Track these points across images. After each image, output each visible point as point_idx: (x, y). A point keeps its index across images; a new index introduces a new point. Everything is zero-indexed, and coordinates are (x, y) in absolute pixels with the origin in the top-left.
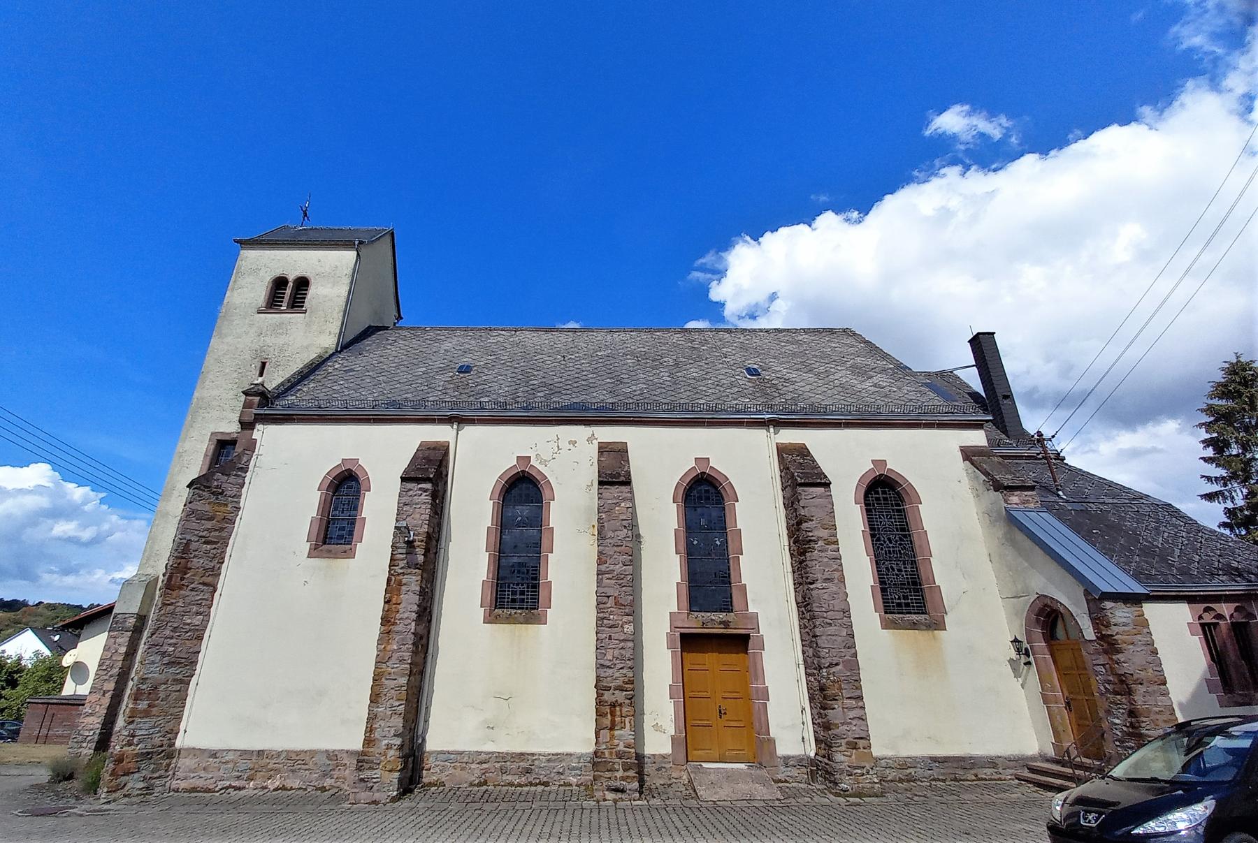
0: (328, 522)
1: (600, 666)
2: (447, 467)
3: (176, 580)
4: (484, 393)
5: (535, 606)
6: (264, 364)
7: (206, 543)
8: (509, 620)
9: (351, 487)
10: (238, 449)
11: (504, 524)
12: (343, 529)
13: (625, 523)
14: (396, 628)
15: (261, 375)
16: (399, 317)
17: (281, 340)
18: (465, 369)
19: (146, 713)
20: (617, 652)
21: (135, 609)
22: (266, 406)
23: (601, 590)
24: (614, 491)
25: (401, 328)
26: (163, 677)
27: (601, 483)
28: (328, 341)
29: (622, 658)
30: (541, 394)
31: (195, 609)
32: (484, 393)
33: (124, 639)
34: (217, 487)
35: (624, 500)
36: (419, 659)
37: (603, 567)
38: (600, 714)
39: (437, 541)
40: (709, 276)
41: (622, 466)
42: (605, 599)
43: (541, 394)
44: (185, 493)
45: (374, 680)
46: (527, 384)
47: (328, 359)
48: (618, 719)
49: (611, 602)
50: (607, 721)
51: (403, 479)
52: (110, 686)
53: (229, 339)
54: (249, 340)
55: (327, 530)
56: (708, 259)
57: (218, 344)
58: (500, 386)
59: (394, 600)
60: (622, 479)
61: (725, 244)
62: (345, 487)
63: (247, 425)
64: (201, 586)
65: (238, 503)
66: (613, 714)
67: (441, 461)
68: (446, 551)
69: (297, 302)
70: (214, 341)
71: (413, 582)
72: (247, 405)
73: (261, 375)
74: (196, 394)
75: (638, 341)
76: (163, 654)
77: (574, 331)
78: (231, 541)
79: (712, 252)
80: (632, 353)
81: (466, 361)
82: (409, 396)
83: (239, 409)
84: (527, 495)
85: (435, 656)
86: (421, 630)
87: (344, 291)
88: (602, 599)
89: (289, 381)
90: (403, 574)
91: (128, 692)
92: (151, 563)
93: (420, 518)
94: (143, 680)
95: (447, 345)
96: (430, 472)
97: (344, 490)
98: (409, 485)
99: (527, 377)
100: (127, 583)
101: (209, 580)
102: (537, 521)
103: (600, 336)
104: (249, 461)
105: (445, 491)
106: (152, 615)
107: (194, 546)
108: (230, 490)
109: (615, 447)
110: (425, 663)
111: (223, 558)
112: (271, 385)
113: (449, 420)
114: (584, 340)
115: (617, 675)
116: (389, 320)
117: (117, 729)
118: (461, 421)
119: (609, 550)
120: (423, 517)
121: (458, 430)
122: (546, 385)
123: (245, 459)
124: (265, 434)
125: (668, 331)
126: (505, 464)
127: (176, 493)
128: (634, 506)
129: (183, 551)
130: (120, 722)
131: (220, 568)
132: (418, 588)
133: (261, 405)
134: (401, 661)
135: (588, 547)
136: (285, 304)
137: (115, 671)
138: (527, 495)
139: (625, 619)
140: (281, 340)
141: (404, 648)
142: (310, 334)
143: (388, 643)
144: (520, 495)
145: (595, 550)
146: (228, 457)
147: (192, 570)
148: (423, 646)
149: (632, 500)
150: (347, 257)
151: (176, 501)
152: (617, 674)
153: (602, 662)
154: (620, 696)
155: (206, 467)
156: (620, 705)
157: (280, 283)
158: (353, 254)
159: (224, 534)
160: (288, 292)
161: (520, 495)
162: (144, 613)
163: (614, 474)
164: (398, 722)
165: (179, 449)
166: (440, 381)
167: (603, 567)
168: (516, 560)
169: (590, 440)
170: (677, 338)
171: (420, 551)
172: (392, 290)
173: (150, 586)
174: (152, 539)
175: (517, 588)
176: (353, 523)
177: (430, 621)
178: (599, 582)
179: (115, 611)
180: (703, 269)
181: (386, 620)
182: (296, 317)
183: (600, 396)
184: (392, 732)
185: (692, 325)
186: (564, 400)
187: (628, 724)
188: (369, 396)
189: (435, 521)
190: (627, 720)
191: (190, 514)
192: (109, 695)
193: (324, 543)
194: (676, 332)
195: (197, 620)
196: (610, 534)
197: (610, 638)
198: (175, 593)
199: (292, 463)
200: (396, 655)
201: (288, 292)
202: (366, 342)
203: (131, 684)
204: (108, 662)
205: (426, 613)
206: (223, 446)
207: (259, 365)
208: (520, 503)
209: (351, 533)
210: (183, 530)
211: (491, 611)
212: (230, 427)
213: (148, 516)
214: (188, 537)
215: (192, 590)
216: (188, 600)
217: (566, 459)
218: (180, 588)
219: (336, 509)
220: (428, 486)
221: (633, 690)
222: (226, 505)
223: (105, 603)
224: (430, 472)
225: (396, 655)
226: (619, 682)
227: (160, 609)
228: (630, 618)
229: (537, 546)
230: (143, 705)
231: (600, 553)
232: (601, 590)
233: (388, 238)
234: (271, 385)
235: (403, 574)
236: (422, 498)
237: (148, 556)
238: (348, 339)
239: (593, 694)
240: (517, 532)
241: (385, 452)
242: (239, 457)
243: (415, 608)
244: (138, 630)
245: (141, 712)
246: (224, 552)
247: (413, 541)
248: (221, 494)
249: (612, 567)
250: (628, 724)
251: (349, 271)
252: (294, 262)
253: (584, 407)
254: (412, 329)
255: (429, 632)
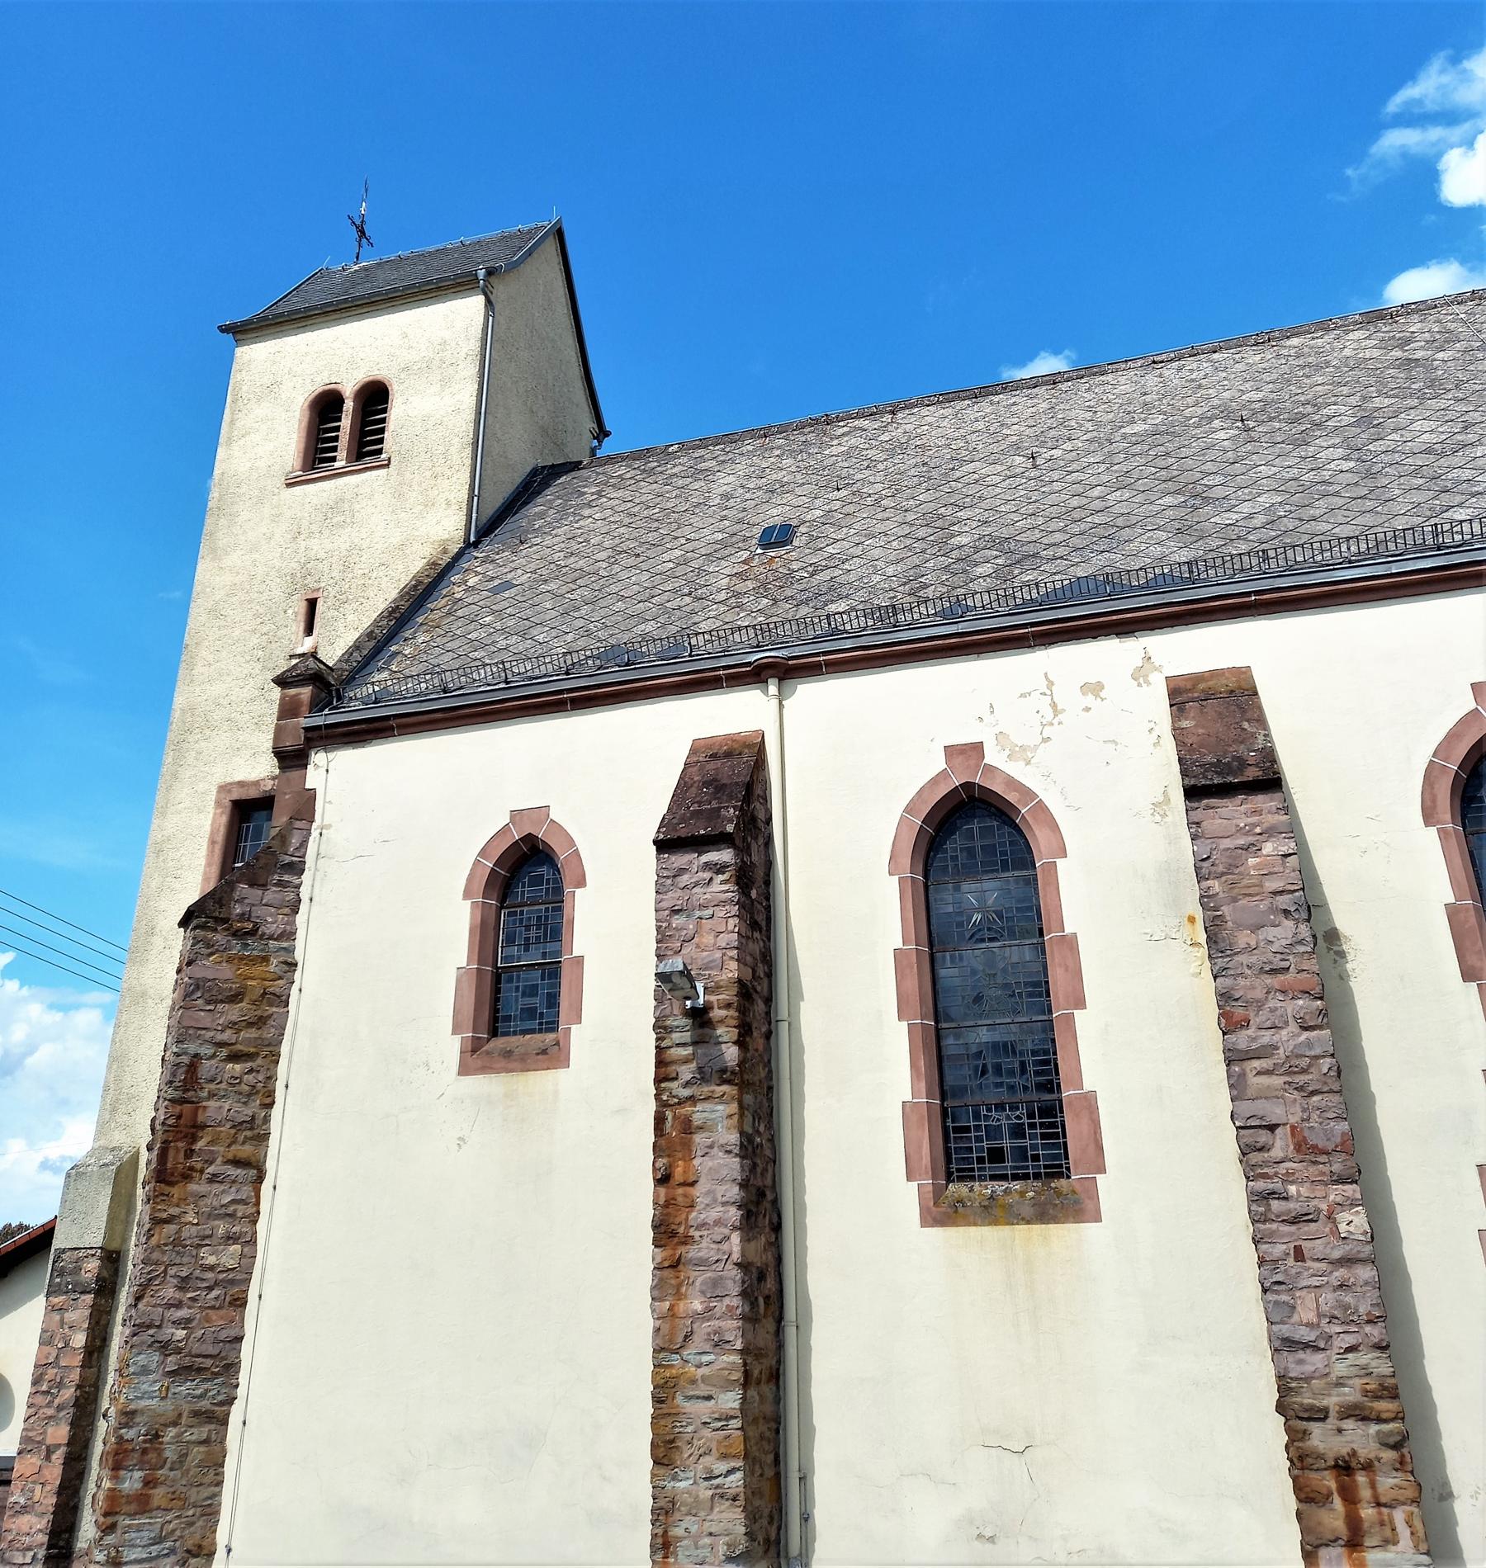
0: (497, 978)
1: (1283, 1345)
2: (766, 799)
3: (175, 1159)
4: (834, 591)
5: (1058, 1169)
6: (312, 604)
7: (234, 1057)
8: (992, 1213)
9: (538, 881)
10: (280, 819)
11: (935, 938)
12: (532, 991)
13: (1284, 901)
14: (692, 1252)
15: (309, 630)
16: (602, 433)
17: (342, 541)
18: (778, 537)
19: (142, 1504)
20: (1328, 1299)
21: (95, 1238)
22: (329, 706)
23: (1247, 1108)
24: (1233, 813)
25: (610, 460)
26: (168, 1405)
27: (1193, 793)
28: (444, 523)
29: (1344, 1317)
30: (987, 569)
31: (222, 1228)
32: (834, 591)
33: (79, 1314)
34: (244, 917)
35: (1270, 832)
36: (764, 1338)
37: (1241, 1040)
38: (1307, 1496)
39: (768, 1035)
40: (1435, 133)
41: (1245, 738)
42: (1263, 1137)
43: (987, 569)
44: (172, 943)
45: (657, 1400)
46: (942, 546)
47: (450, 567)
48: (1367, 1512)
49: (1281, 1145)
50: (1334, 1517)
51: (664, 846)
52: (60, 1433)
53: (233, 559)
54: (293, 550)
55: (496, 1000)
56: (1427, 87)
57: (213, 576)
58: (869, 563)
59: (678, 1174)
60: (1252, 774)
61: (1043, 349)
62: (526, 877)
63: (292, 758)
64: (233, 1172)
65: (291, 950)
66: (1350, 1497)
67: (749, 787)
68: (794, 1028)
69: (368, 445)
70: (205, 570)
71: (718, 1119)
72: (288, 710)
73: (309, 630)
74: (179, 701)
75: (1236, 376)
76: (165, 1347)
77: (1052, 380)
78: (285, 1049)
79: (1437, 63)
80: (1225, 413)
81: (775, 515)
82: (649, 627)
83: (271, 720)
84: (989, 850)
85: (804, 1327)
86: (758, 1257)
87: (465, 394)
88: (1252, 1137)
89: (370, 635)
90: (692, 1100)
91: (98, 1448)
92: (121, 1118)
93: (716, 944)
94: (128, 1417)
95: (726, 481)
96: (725, 818)
97: (524, 891)
98: (679, 860)
99: (940, 529)
100: (76, 1174)
101: (245, 1150)
102: (1028, 919)
103: (1123, 383)
104: (304, 844)
105: (769, 864)
106: (134, 1253)
107: (207, 1068)
108: (272, 924)
109: (1220, 685)
110: (780, 1346)
111: (271, 1094)
112: (332, 654)
113: (755, 675)
114: (1082, 404)
115: (1343, 1372)
116: (578, 448)
117: (81, 1545)
118: (785, 672)
119: (1251, 986)
120: (723, 941)
121: (781, 698)
122: (995, 542)
123: (295, 841)
124: (333, 773)
125: (1324, 327)
126: (914, 773)
127: (158, 941)
128: (1302, 851)
129: (185, 1083)
130: (88, 1529)
131: (267, 1120)
132: (733, 1138)
133: (317, 706)
134: (719, 1344)
135: (1189, 981)
136: (342, 455)
137: (68, 1394)
138: (989, 850)
139: (1336, 1193)
140: (342, 541)
141: (720, 1307)
142: (408, 510)
143: (679, 1296)
144: (971, 852)
145: (1205, 990)
146: (260, 838)
147: (207, 1129)
148: (767, 1296)
149: (1293, 830)
150: (461, 318)
151: (166, 949)
152: (1340, 1369)
153: (1285, 1330)
154: (1361, 1439)
155: (215, 871)
156: (1368, 1467)
157: (326, 406)
158: (478, 301)
159: (268, 1033)
160: (346, 422)
161: (971, 852)
162: (114, 1246)
163: (1228, 763)
164: (731, 1521)
165: (155, 835)
166: (721, 575)
167: (1241, 1040)
168: (984, 1036)
169: (1139, 675)
170: (1357, 343)
171: (726, 1033)
172: (576, 371)
173: (124, 1175)
174: (117, 1060)
175: (1003, 1127)
176: (552, 971)
177: (777, 1228)
178: (1237, 1087)
179: (58, 1243)
180: (1413, 118)
181: (666, 1231)
182: (367, 483)
183: (1153, 549)
184: (722, 1549)
185: (1410, 287)
186: (1050, 576)
187: (1403, 1532)
188: (555, 646)
189: (755, 948)
190: (1399, 1516)
191: (194, 991)
192: (58, 1457)
193: (494, 1033)
194: (1346, 326)
195: (230, 1256)
196: (1244, 939)
197: (1299, 1254)
198: (175, 1191)
199: (402, 830)
200: (703, 1329)
201: (346, 422)
202: (534, 509)
203: (102, 1426)
204: (51, 1372)
205: (765, 1206)
206: (247, 813)
207: (302, 608)
208: (970, 871)
209: (553, 1001)
210: (181, 1033)
211: (938, 1193)
212: (257, 767)
213: (108, 997)
214: (192, 1048)
215: (213, 1179)
216: (205, 1205)
217: (1083, 735)
218: (187, 1177)
219: (510, 940)
220: (725, 855)
221: (1399, 1417)
222: (265, 960)
223: (35, 1220)
224: (725, 818)
225: (703, 1329)
226: (1350, 1394)
227: (149, 1234)
228: (1351, 1190)
229: (1040, 989)
230: (132, 1482)
231: (1224, 997)
232: (1247, 1108)
233: (551, 246)
234: (332, 654)
235: (692, 1100)
236: (712, 885)
237: (113, 1104)
238: (490, 510)
239: (1274, 1432)
240: (974, 956)
241: (609, 778)
242: (283, 838)
243: (734, 1192)
244: (106, 1288)
245: (130, 1499)
246: (271, 1078)
247: (707, 1008)
248: (253, 933)
249: (1267, 1038)
250: (1403, 1532)
251: (474, 345)
252: (342, 353)
253: (1108, 584)
254: (635, 456)
255: (779, 1260)
